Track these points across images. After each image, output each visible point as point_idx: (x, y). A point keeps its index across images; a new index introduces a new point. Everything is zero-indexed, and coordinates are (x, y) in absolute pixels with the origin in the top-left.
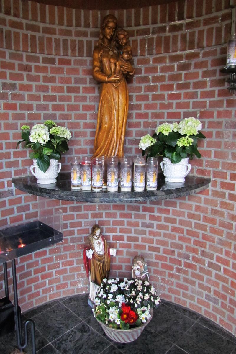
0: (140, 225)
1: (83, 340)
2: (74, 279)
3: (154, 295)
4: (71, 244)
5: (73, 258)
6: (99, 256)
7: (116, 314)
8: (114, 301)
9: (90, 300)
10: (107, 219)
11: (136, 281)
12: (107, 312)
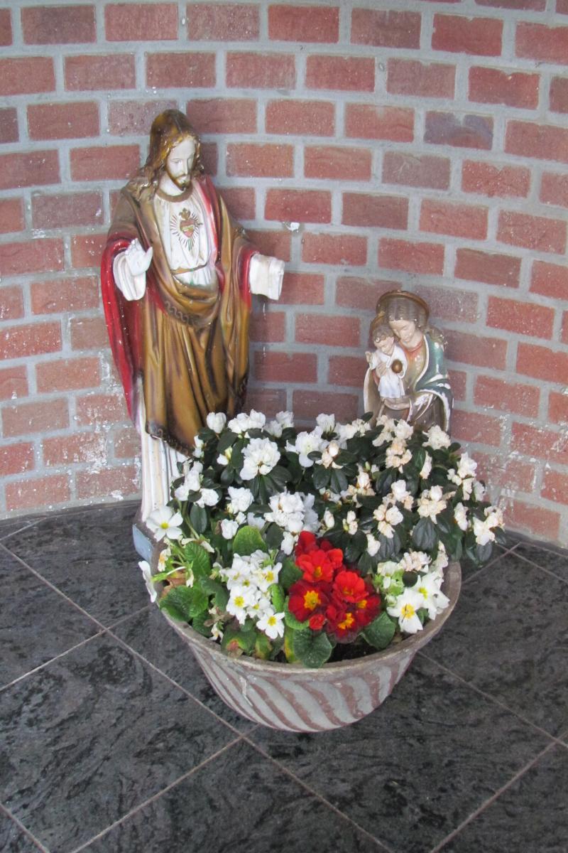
0: (420, 129)
1: (97, 717)
2: (65, 424)
3: (472, 495)
4: (40, 234)
5: (54, 310)
6: (184, 294)
7: (264, 587)
8: (259, 523)
9: (147, 533)
10: (236, 94)
11: (382, 427)
12: (218, 579)
